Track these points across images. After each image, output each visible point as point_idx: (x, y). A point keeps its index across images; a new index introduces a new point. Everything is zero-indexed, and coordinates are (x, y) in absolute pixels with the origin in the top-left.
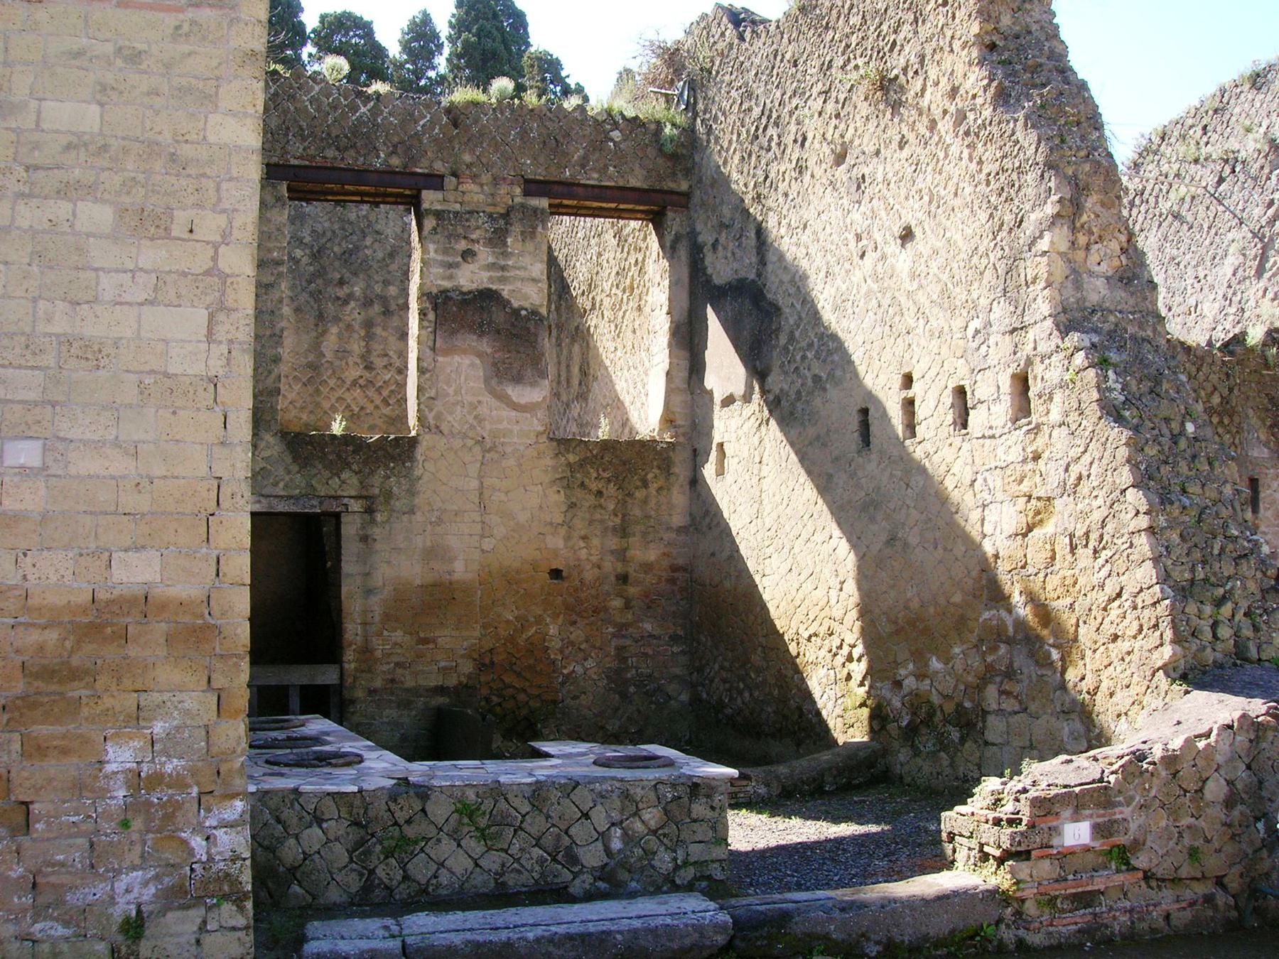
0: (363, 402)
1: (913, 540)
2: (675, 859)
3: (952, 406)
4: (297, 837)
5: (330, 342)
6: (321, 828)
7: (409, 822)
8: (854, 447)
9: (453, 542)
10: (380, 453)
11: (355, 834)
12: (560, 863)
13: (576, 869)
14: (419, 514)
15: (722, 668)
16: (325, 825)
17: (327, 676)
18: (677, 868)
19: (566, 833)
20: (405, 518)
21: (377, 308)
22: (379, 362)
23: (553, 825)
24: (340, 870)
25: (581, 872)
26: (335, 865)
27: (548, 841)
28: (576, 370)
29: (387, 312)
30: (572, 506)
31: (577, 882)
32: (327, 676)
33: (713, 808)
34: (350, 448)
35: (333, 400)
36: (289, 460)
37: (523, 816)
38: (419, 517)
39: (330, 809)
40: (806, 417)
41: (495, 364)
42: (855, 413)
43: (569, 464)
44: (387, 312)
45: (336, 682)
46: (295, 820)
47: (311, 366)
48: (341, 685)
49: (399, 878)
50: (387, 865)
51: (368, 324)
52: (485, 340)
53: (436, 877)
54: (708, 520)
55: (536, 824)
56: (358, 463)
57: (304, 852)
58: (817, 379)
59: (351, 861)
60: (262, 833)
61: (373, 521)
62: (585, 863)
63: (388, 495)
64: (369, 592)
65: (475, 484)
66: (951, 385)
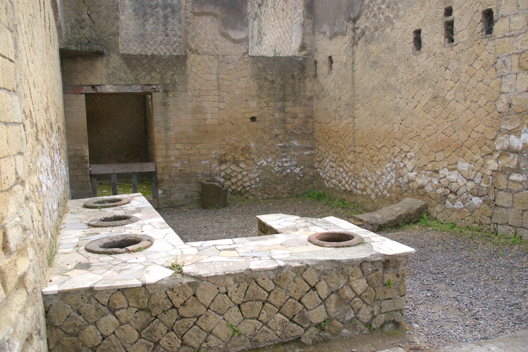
0: (165, 50)
1: (449, 96)
2: (372, 312)
3: (481, 21)
4: (95, 324)
5: (149, 27)
6: (115, 315)
7: (183, 305)
8: (411, 51)
9: (205, 104)
10: (170, 63)
11: (143, 317)
12: (295, 322)
13: (306, 326)
14: (189, 92)
15: (331, 161)
16: (117, 313)
17: (149, 167)
18: (374, 317)
19: (299, 301)
20: (183, 94)
21: (169, 10)
22: (171, 33)
23: (291, 297)
24: (132, 345)
25: (309, 327)
26: (128, 342)
27: (288, 309)
28: (256, 32)
29: (174, 11)
30: (260, 88)
31: (307, 333)
32: (149, 167)
33: (398, 276)
34: (155, 61)
35: (153, 50)
36: (126, 67)
37: (269, 293)
38: (189, 93)
39: (120, 300)
40: (381, 38)
41: (222, 20)
42: (412, 33)
43: (259, 68)
44: (174, 11)
45: (154, 170)
46: (93, 312)
47: (142, 35)
48: (156, 172)
49: (179, 345)
50: (168, 337)
51: (166, 17)
52: (218, 8)
53: (206, 341)
54: (323, 93)
55: (278, 298)
56: (159, 68)
57: (102, 335)
58: (387, 18)
59: (140, 337)
60: (66, 324)
61: (168, 95)
62: (313, 321)
63: (174, 84)
64: (167, 129)
65: (215, 77)
66: (481, 9)
